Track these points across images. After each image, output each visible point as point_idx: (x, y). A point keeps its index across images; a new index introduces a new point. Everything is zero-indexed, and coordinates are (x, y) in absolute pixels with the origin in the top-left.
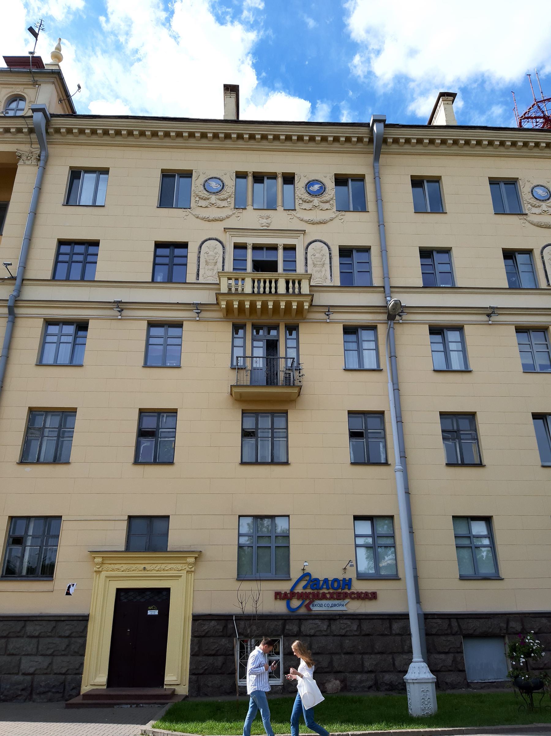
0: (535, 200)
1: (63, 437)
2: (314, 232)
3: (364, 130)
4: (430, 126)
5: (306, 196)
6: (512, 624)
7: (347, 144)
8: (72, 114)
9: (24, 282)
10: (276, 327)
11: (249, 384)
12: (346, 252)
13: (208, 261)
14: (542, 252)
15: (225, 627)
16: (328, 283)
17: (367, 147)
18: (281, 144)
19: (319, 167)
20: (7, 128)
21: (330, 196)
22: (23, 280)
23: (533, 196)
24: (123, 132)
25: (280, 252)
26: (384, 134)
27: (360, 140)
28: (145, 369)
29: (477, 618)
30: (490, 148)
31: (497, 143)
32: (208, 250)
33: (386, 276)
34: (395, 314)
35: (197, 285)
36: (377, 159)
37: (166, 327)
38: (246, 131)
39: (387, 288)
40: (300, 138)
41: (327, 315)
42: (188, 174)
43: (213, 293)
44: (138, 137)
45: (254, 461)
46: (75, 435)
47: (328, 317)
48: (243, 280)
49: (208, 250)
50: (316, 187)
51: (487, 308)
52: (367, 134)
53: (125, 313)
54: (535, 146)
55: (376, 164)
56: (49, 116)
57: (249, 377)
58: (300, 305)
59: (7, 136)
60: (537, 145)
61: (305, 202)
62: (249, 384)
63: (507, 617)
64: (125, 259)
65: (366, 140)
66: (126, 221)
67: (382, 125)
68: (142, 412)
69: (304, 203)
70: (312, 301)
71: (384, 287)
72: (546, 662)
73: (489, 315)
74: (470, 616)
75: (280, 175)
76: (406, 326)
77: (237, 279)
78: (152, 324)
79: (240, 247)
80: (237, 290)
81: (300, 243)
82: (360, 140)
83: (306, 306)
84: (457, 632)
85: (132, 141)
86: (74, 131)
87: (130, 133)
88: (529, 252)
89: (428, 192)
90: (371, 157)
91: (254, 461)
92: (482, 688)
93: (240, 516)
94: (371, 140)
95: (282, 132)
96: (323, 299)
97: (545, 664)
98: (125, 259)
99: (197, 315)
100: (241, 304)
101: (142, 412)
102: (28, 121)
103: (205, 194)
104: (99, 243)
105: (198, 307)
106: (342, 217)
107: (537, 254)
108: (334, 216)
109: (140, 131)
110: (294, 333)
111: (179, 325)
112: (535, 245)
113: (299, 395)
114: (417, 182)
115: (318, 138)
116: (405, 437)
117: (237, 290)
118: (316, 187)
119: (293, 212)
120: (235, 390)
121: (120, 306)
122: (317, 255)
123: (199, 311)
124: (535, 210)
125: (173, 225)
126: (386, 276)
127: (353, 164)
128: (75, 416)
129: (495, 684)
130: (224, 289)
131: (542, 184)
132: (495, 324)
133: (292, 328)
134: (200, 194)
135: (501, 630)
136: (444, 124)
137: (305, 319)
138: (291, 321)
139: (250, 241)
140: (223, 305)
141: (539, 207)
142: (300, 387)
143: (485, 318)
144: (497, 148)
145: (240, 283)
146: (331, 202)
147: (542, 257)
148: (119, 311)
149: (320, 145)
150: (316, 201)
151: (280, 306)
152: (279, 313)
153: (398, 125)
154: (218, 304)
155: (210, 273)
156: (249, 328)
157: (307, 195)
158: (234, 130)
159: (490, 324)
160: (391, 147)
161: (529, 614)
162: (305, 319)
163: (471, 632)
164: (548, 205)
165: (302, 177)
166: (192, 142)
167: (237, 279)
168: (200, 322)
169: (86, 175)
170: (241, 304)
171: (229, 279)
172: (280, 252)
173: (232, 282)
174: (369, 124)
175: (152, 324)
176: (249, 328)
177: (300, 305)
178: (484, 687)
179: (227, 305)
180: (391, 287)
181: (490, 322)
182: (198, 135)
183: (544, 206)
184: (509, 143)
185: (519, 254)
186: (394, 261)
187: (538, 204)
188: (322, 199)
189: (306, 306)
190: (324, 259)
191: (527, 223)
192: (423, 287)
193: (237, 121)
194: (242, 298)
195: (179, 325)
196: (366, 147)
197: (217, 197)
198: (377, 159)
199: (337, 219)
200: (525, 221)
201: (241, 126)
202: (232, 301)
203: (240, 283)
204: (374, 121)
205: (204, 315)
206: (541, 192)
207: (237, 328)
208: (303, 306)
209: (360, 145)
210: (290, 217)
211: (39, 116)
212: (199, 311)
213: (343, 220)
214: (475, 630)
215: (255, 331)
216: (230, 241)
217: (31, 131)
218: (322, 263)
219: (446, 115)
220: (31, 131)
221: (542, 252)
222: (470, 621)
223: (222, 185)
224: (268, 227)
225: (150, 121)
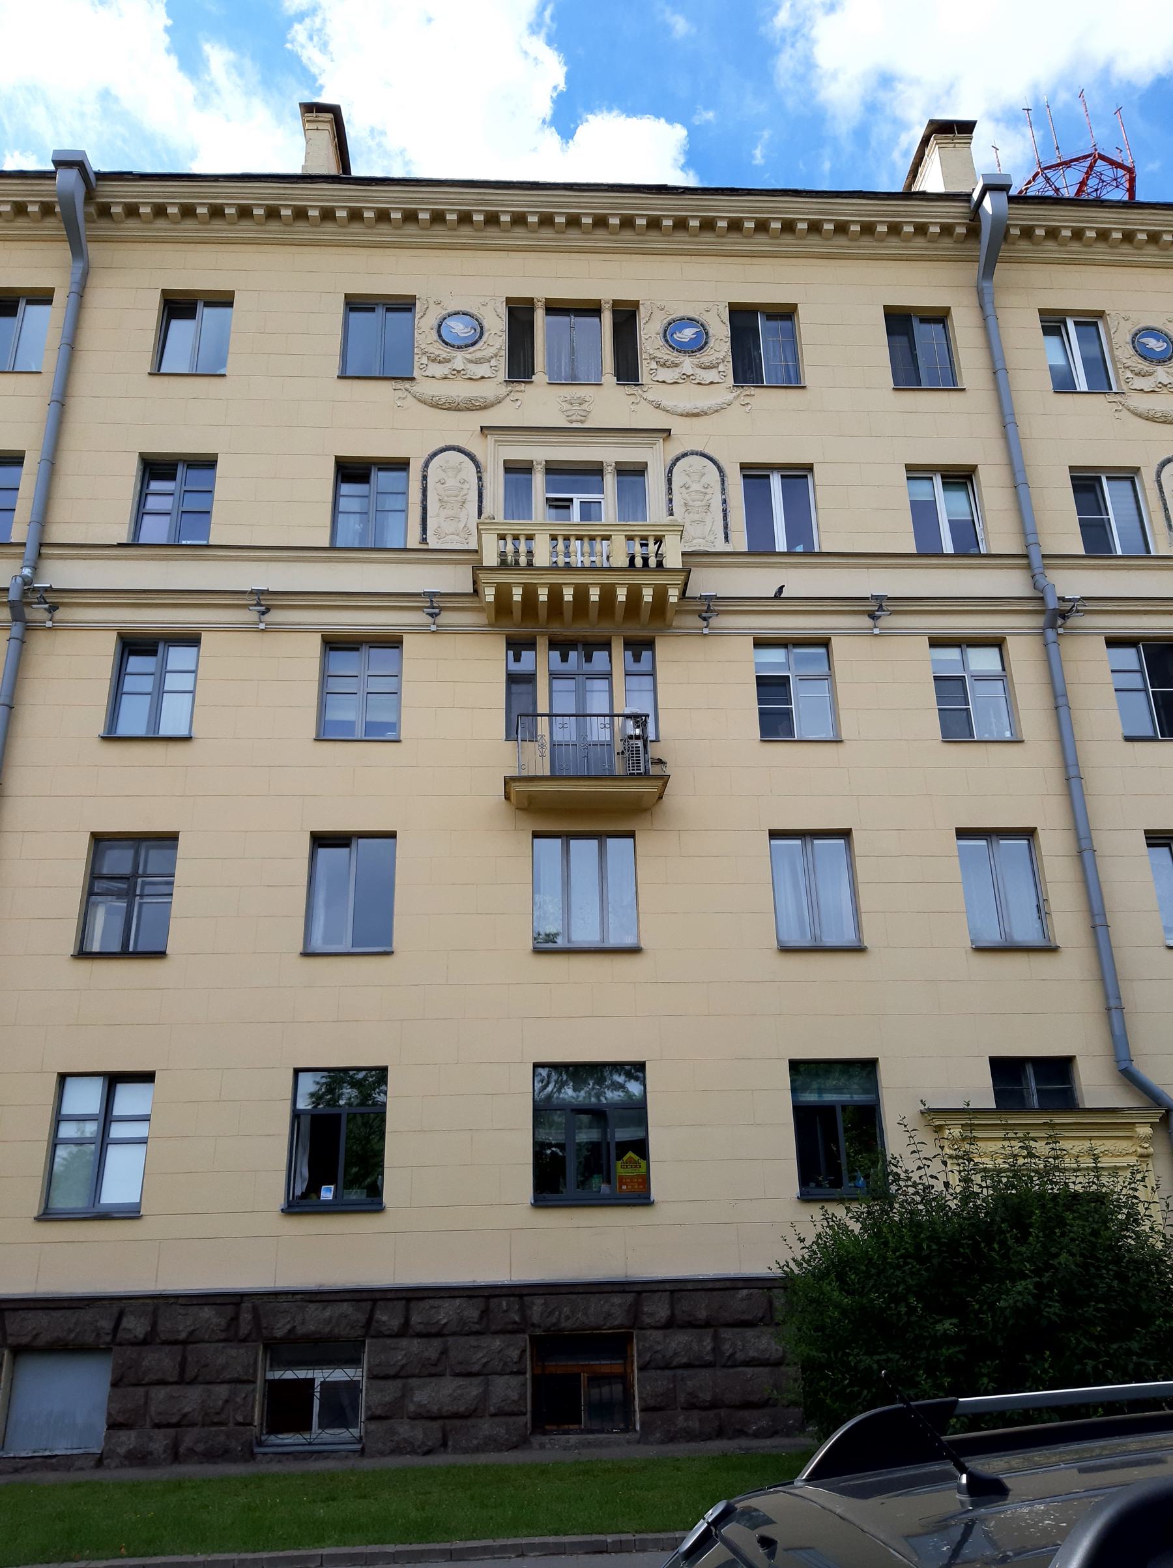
0: (442, 346)
1: (141, 896)
2: (687, 435)
3: (958, 208)
4: (908, 195)
5: (666, 354)
6: (129, 1322)
7: (677, 234)
8: (344, 176)
9: (44, 551)
10: (605, 645)
11: (547, 773)
12: (755, 475)
13: (691, 503)
14: (426, 465)
15: (232, 1319)
16: (721, 546)
17: (963, 246)
18: (474, 234)
19: (687, 288)
20: (410, 210)
21: (717, 355)
22: (41, 545)
23: (440, 336)
24: (339, 214)
25: (610, 480)
26: (1009, 219)
27: (947, 230)
28: (318, 744)
29: (49, 1309)
30: (814, 239)
31: (1117, 235)
32: (686, 479)
33: (42, 519)
34: (1057, 617)
35: (425, 553)
36: (78, 251)
37: (964, 647)
38: (369, 201)
39: (1036, 561)
40: (573, 221)
41: (705, 619)
42: (404, 305)
43: (468, 570)
44: (39, 216)
45: (117, 948)
46: (176, 891)
47: (705, 623)
48: (530, 538)
49: (686, 479)
50: (688, 333)
51: (867, 598)
52: (965, 218)
53: (60, 614)
54: (1071, 238)
55: (986, 284)
56: (92, 177)
57: (547, 759)
58: (661, 593)
59: (837, 243)
60: (1078, 234)
61: (663, 365)
62: (547, 773)
63: (120, 1305)
64: (271, 497)
65: (961, 230)
66: (276, 409)
67: (1003, 197)
68: (99, 840)
69: (660, 368)
70: (686, 584)
71: (1026, 556)
72: (186, 1410)
73: (872, 616)
74: (32, 1305)
75: (607, 306)
76: (63, 636)
77: (516, 538)
78: (334, 644)
79: (517, 470)
80: (645, 560)
81: (655, 457)
82: (947, 230)
83: (673, 595)
84: (249, 1335)
85: (443, 236)
86: (365, 215)
87: (492, 219)
88: (401, 465)
89: (757, 343)
90: (972, 271)
91: (117, 948)
92: (16, 1471)
93: (63, 1077)
94: (974, 231)
95: (259, 198)
96: (706, 582)
97: (185, 1415)
98: (271, 497)
99: (430, 620)
100: (530, 593)
101: (99, 840)
102: (45, 186)
103: (443, 352)
104: (408, 464)
105: (433, 604)
106: (748, 400)
107: (1147, 477)
108: (730, 397)
109: (460, 212)
110: (646, 654)
111: (393, 642)
112: (414, 450)
113: (661, 798)
114: (899, 321)
115: (506, 218)
116: (1103, 885)
117: (645, 560)
118: (688, 333)
119: (407, 385)
120: (518, 787)
121: (264, 601)
122: (451, 482)
123: (437, 611)
124: (1139, 383)
125: (377, 422)
126: (42, 519)
127: (921, 284)
128: (175, 847)
129: (54, 1460)
130: (490, 558)
131: (467, 310)
132: (887, 633)
133: (640, 646)
134: (430, 349)
135: (98, 1335)
136: (941, 189)
137: (670, 627)
138: (637, 631)
139: (539, 453)
140: (489, 594)
141: (447, 361)
142: (665, 779)
143: (866, 622)
144: (882, 241)
145: (652, 547)
146: (721, 368)
147: (425, 478)
148: (432, 615)
149: (619, 237)
150: (687, 364)
151: (511, 595)
152: (510, 612)
153: (130, 173)
154: (476, 592)
155: (448, 527)
156: (542, 643)
157: (668, 350)
158: (342, 198)
159: (262, 630)
160: (1016, 247)
161: (177, 1297)
162: (670, 627)
163: (25, 1340)
164: (468, 356)
165: (432, 306)
166: (245, 228)
167: (516, 538)
168: (266, 634)
169: (30, 308)
170: (530, 593)
171: (630, 538)
172: (610, 480)
173: (637, 549)
174: (970, 195)
175: (334, 644)
176: (542, 643)
177: (661, 593)
178: (23, 1468)
179: (496, 596)
180: (1044, 556)
181: (876, 631)
182: (641, 222)
183: (1162, 373)
184: (1119, 235)
185: (380, 469)
186: (69, 484)
187: (444, 355)
188: (702, 360)
189: (673, 595)
190: (465, 492)
191: (1125, 412)
192: (749, 554)
193: (1132, 204)
194: (660, 579)
195: (393, 642)
196: (959, 246)
197: (696, 361)
198: (988, 271)
199: (737, 403)
200: (406, 393)
201: (1146, 215)
202: (509, 586)
203: (652, 547)
204: (986, 189)
205: (446, 618)
206: (462, 327)
207: (517, 646)
208: (588, 596)
209: (947, 242)
210: (632, 398)
211: (68, 179)
212: (437, 611)
213: (519, 403)
214: (36, 1336)
215: (511, 653)
216: (495, 455)
217: (47, 210)
218: (704, 503)
219: (307, 153)
220: (47, 210)
221: (426, 465)
222: (30, 1314)
223: (478, 330)
224: (582, 422)
225: (9, 181)
